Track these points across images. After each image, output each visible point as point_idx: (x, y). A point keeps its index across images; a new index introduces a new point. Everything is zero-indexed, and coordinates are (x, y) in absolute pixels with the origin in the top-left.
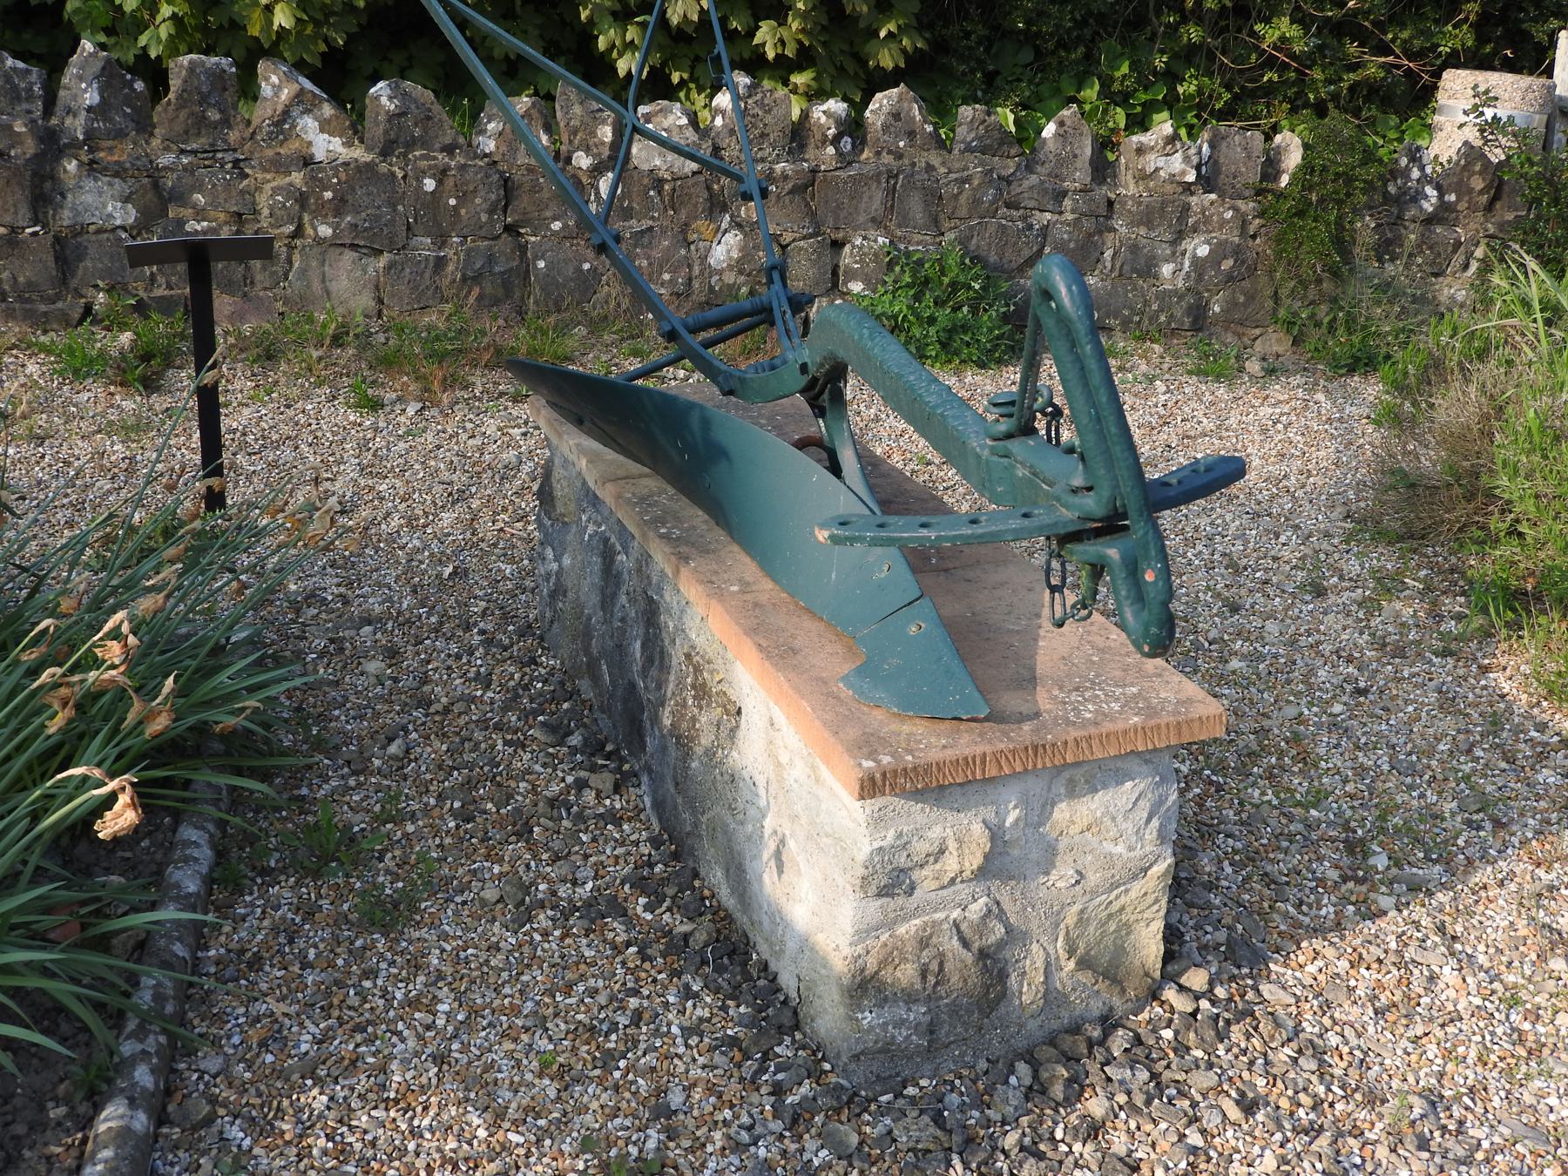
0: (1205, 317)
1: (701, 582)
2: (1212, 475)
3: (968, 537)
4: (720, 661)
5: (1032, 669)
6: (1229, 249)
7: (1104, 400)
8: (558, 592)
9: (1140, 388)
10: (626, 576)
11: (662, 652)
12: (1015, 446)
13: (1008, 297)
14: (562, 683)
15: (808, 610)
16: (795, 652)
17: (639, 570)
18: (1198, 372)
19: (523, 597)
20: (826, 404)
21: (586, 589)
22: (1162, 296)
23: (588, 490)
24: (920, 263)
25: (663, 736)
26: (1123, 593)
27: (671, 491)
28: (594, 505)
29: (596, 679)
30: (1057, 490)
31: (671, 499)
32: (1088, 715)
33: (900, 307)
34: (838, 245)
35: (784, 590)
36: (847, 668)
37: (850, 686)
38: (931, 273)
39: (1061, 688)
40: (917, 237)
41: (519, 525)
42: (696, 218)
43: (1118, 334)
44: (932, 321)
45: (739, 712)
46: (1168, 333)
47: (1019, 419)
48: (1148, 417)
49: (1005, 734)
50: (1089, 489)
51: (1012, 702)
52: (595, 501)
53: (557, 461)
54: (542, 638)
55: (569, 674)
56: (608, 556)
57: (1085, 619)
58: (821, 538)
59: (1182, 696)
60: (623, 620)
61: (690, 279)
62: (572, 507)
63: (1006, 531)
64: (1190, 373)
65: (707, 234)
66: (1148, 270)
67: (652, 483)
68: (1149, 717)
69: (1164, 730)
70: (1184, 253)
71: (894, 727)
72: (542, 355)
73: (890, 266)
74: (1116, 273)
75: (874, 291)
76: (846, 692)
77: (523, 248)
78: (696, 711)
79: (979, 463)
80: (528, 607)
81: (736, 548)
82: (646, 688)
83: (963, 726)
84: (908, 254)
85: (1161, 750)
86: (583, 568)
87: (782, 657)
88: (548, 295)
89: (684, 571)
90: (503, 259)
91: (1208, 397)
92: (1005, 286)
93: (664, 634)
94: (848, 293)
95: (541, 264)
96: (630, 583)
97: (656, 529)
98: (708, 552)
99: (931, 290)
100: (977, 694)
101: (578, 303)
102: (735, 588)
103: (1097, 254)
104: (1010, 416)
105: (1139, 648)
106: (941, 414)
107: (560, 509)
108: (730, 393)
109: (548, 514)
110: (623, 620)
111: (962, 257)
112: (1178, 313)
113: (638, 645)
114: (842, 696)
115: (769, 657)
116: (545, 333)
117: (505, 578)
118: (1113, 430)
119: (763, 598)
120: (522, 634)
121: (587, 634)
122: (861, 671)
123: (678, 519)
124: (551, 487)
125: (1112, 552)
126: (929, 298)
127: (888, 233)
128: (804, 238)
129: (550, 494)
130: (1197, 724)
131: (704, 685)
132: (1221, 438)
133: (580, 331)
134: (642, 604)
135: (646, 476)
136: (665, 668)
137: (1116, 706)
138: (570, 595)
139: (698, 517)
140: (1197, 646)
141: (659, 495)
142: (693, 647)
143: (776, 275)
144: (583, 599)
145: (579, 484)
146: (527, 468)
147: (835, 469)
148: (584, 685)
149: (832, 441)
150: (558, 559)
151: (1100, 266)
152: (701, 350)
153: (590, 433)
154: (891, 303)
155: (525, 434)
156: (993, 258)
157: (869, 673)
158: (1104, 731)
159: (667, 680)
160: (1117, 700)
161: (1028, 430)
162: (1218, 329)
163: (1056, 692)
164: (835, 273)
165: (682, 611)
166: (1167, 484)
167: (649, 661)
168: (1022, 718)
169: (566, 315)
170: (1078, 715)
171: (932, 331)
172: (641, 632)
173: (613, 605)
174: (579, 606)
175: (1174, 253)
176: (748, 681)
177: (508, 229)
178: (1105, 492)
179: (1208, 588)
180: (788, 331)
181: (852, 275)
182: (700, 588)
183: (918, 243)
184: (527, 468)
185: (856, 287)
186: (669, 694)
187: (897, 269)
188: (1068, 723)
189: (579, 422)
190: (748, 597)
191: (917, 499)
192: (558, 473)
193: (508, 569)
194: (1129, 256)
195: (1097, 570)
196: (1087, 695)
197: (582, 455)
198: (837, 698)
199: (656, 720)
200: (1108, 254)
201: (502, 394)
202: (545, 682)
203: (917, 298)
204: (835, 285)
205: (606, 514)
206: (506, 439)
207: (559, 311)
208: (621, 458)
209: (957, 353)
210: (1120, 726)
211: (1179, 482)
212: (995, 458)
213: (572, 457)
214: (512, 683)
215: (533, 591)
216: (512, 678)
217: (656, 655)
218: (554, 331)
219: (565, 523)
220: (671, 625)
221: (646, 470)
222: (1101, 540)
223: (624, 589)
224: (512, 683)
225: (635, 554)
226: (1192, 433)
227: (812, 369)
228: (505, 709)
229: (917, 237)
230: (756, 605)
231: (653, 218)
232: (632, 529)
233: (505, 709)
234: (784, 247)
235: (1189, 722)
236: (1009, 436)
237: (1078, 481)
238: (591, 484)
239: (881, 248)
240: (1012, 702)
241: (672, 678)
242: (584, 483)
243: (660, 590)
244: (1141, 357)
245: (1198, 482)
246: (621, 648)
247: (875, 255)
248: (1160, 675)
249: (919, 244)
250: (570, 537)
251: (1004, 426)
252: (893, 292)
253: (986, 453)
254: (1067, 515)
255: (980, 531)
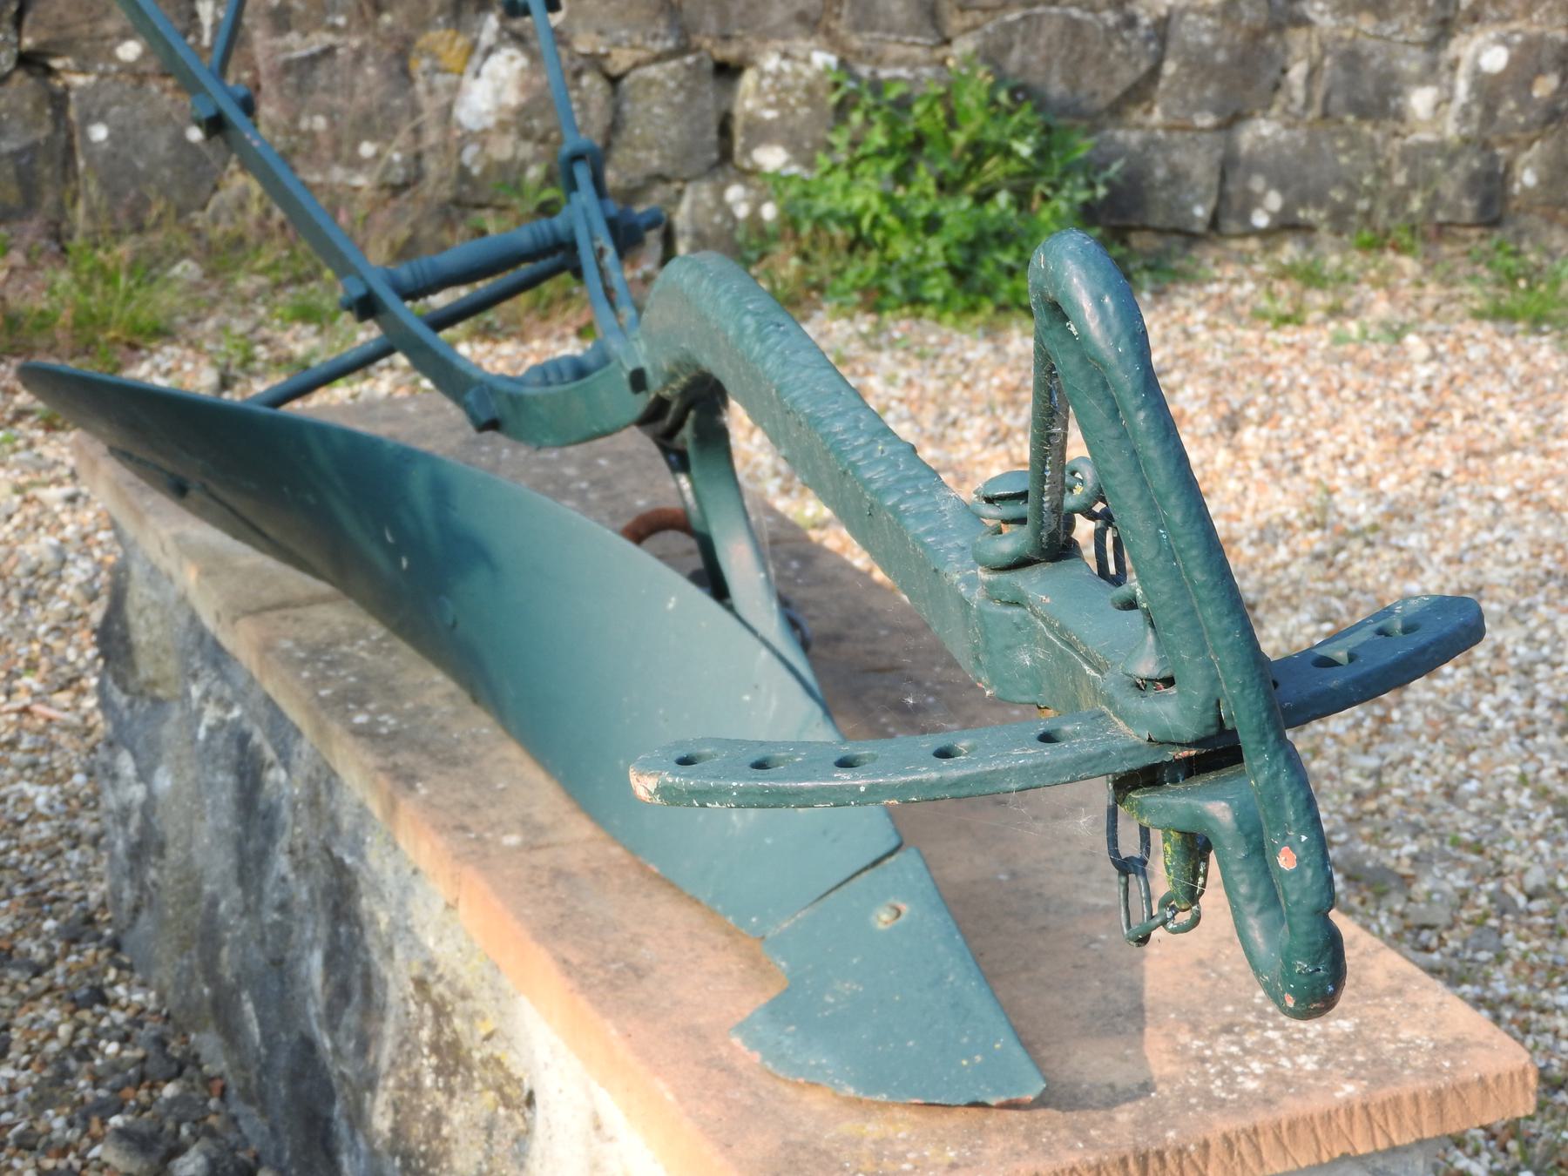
0: (1506, 198)
1: (440, 829)
2: (1420, 638)
3: (934, 785)
4: (487, 994)
5: (1136, 990)
6: (1547, 55)
7: (1177, 517)
8: (146, 848)
9: (1374, 352)
10: (286, 814)
11: (367, 976)
12: (1036, 585)
13: (1092, 168)
14: (161, 1042)
15: (666, 883)
16: (639, 972)
17: (313, 803)
18: (1498, 314)
19: (75, 856)
20: (690, 448)
21: (204, 840)
22: (1415, 156)
23: (202, 634)
24: (904, 104)
25: (374, 1154)
26: (1244, 889)
27: (377, 631)
28: (216, 665)
29: (231, 1032)
30: (1107, 682)
31: (376, 648)
32: (1251, 1085)
33: (865, 196)
34: (727, 72)
35: (615, 839)
36: (751, 1002)
37: (756, 1043)
38: (926, 125)
39: (1195, 1028)
40: (895, 51)
41: (64, 698)
42: (425, 25)
43: (1324, 235)
44: (932, 224)
45: (530, 1100)
46: (1432, 233)
47: (1037, 533)
48: (1393, 416)
49: (1080, 1133)
50: (1169, 682)
51: (1093, 1062)
52: (218, 657)
53: (136, 569)
54: (116, 945)
55: (174, 1021)
56: (249, 772)
57: (1185, 929)
58: (641, 792)
59: (1444, 1035)
60: (283, 907)
61: (418, 157)
62: (171, 666)
63: (1008, 771)
64: (1478, 315)
65: (451, 58)
66: (1380, 102)
67: (337, 617)
68: (1377, 1081)
69: (1408, 1109)
70: (1454, 66)
71: (848, 1127)
72: (105, 326)
73: (842, 110)
74: (1315, 112)
75: (810, 164)
76: (745, 1055)
77: (59, 101)
78: (441, 1099)
79: (966, 616)
80: (87, 877)
81: (513, 751)
82: (337, 1051)
83: (992, 1119)
84: (877, 87)
85: (1406, 1149)
86: (197, 797)
87: (613, 986)
88: (116, 195)
89: (407, 807)
90: (17, 125)
91: (1517, 367)
92: (1083, 147)
93: (370, 939)
94: (755, 171)
95: (99, 133)
96: (294, 830)
97: (346, 715)
98: (454, 762)
99: (931, 160)
100: (1017, 1052)
101: (181, 212)
102: (513, 840)
103: (1273, 74)
104: (1021, 521)
105: (1276, 998)
106: (894, 509)
107: (146, 670)
108: (493, 425)
109: (120, 680)
110: (283, 907)
111: (993, 89)
112: (1449, 188)
113: (316, 960)
114: (740, 1064)
115: (585, 987)
116: (110, 279)
117: (35, 816)
118: (1199, 576)
119: (573, 859)
120: (73, 937)
121: (209, 937)
122: (777, 1011)
123: (392, 693)
124: (125, 625)
125: (1217, 809)
126: (924, 178)
127: (833, 42)
128: (658, 59)
129: (125, 639)
130: (1476, 1092)
131: (455, 1045)
132: (1546, 454)
133: (187, 270)
134: (322, 874)
135: (324, 600)
136: (372, 1006)
137: (1308, 1063)
138: (173, 853)
139: (433, 687)
140: (1502, 904)
141: (353, 639)
142: (430, 965)
143: (582, 173)
144: (199, 861)
145: (183, 620)
146: (79, 571)
147: (714, 582)
148: (207, 1043)
149: (705, 521)
150: (144, 775)
151: (1281, 98)
152: (424, 332)
153: (201, 512)
154: (846, 190)
155: (72, 499)
156: (1056, 88)
157: (793, 1011)
158: (1284, 1116)
159: (379, 1035)
160: (1311, 1048)
161: (1059, 549)
162: (1535, 220)
163: (1184, 1037)
164: (725, 128)
165: (406, 890)
166: (1327, 663)
167: (341, 994)
168: (1114, 1098)
169: (156, 238)
170: (1230, 1087)
171: (935, 246)
172: (323, 932)
173: (262, 874)
174: (191, 879)
175: (1433, 67)
176: (545, 1037)
177: (26, 60)
178: (1194, 689)
179: (1523, 779)
180: (608, 292)
181: (761, 133)
182: (441, 842)
183: (899, 62)
184: (79, 571)
185: (772, 158)
186: (384, 1064)
187: (856, 118)
188: (1211, 1102)
189: (179, 490)
190: (541, 858)
191: (894, 629)
192: (139, 594)
193: (41, 796)
194: (1341, 76)
195: (1196, 846)
196: (1250, 1040)
197: (188, 560)
198: (728, 1070)
199: (358, 1118)
200: (1297, 72)
201: (21, 414)
202: (125, 1040)
203: (902, 176)
204: (726, 155)
205: (241, 682)
206: (32, 511)
207: (139, 229)
208: (269, 563)
209: (988, 291)
210: (1317, 1104)
211: (1352, 657)
212: (995, 608)
213: (167, 564)
214: (53, 1046)
215: (95, 841)
216: (53, 1035)
217: (353, 982)
218: (131, 272)
219: (157, 701)
220: (383, 919)
221: (323, 587)
222: (1197, 782)
223: (283, 842)
224: (53, 1046)
225: (303, 767)
226: (1485, 446)
227: (655, 384)
228: (40, 1103)
229: (895, 51)
230: (558, 874)
231: (334, 28)
232: (295, 714)
233: (40, 1103)
234: (614, 81)
235: (1460, 1090)
236: (1020, 563)
237: (1147, 667)
238: (208, 621)
239: (821, 74)
240: (1093, 1062)
241: (389, 1029)
242: (194, 618)
243: (357, 847)
244: (1375, 284)
245: (1402, 648)
246: (281, 966)
247: (810, 90)
248: (1399, 992)
249: (903, 64)
250: (168, 731)
251: (1012, 542)
252: (851, 167)
253: (977, 597)
254: (1131, 732)
255: (955, 773)
